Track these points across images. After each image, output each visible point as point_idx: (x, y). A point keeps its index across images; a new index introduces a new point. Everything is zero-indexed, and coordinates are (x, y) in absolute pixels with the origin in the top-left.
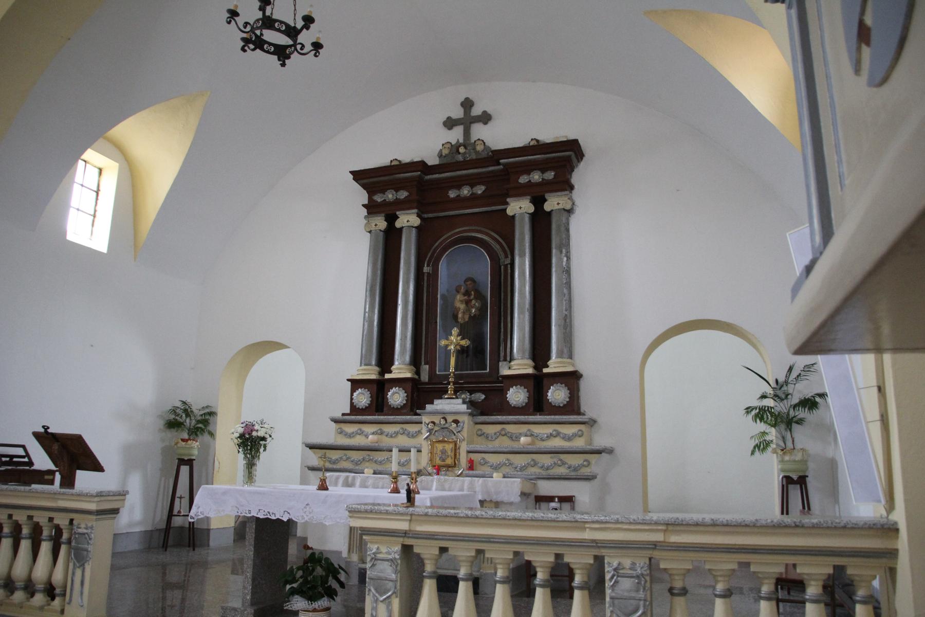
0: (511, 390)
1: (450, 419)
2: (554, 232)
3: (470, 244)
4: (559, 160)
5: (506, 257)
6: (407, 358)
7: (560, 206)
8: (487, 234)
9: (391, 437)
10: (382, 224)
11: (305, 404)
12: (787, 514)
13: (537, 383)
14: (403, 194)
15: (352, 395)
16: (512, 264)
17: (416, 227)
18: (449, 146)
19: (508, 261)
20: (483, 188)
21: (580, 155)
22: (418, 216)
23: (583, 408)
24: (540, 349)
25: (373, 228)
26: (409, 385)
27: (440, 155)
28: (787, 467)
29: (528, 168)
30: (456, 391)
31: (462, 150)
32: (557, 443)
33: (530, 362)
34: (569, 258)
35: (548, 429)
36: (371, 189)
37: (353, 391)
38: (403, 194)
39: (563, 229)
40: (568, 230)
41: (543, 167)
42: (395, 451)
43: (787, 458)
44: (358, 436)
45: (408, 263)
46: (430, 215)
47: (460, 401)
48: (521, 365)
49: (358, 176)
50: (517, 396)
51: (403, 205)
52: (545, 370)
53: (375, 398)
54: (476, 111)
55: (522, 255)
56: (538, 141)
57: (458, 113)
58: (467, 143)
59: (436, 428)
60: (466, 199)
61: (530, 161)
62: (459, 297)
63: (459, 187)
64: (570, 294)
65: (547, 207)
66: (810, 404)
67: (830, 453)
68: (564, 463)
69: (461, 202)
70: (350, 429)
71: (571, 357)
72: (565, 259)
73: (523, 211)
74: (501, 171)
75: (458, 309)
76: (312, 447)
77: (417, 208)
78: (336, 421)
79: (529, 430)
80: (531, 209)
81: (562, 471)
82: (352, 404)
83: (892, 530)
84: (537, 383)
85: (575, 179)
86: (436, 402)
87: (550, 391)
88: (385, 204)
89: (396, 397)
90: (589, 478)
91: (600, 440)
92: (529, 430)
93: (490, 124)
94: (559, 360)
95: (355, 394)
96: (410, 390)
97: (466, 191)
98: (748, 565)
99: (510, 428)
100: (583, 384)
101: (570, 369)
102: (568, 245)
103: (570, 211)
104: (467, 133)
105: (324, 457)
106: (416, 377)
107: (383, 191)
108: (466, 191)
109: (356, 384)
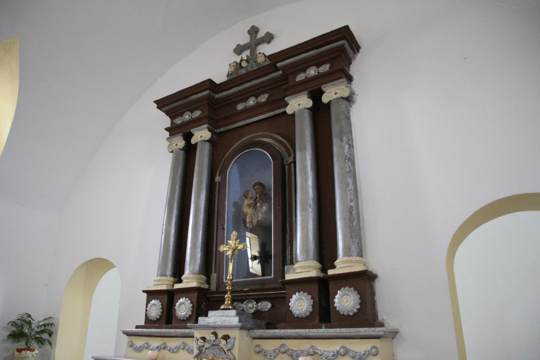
0: (294, 297)
1: (220, 334)
5: (290, 155)
7: (338, 95)
9: (173, 352)
10: (180, 142)
13: (323, 288)
14: (197, 114)
15: (147, 306)
17: (208, 141)
20: (266, 96)
21: (356, 47)
22: (210, 130)
23: (382, 315)
24: (326, 252)
26: (195, 295)
29: (303, 66)
30: (233, 301)
31: (244, 64)
33: (318, 265)
34: (351, 146)
36: (172, 114)
38: (197, 114)
39: (342, 116)
40: (349, 118)
41: (317, 62)
44: (145, 350)
46: (222, 129)
48: (304, 267)
49: (155, 102)
50: (300, 304)
51: (196, 123)
52: (331, 272)
54: (261, 35)
55: (304, 149)
59: (207, 345)
61: (304, 59)
63: (245, 100)
64: (355, 183)
65: (325, 99)
72: (347, 147)
73: (302, 107)
74: (282, 76)
75: (245, 215)
77: (207, 123)
78: (129, 334)
79: (312, 347)
80: (309, 103)
85: (353, 70)
86: (211, 313)
87: (337, 296)
89: (183, 307)
92: (312, 347)
94: (347, 258)
96: (195, 300)
99: (291, 344)
100: (379, 286)
101: (358, 268)
103: (349, 99)
106: (206, 286)
108: (251, 102)
109: (151, 294)
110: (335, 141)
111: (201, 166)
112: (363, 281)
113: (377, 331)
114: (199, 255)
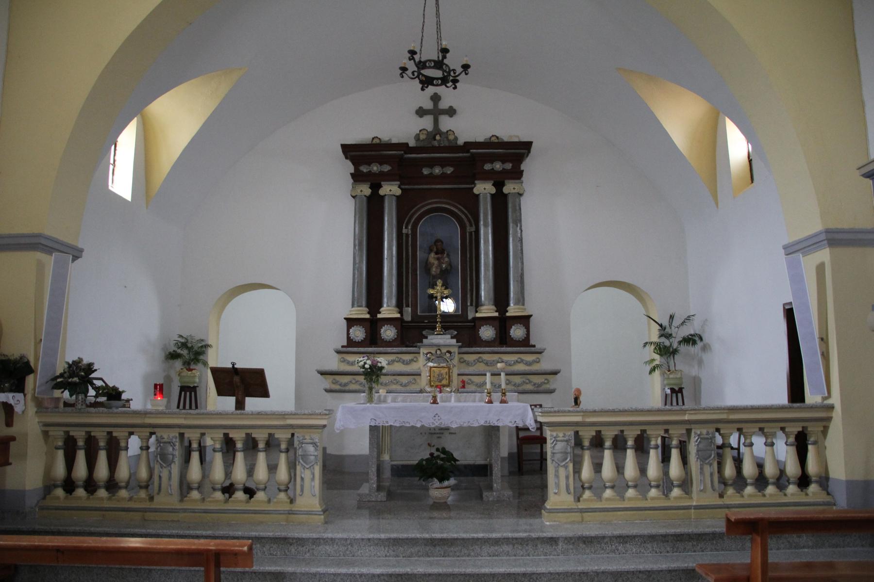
1: (444, 350)
2: (510, 210)
3: (437, 216)
4: (515, 153)
6: (394, 301)
7: (516, 191)
8: (457, 208)
10: (366, 190)
11: (297, 340)
12: (197, 407)
13: (503, 323)
14: (386, 168)
16: (477, 232)
18: (425, 132)
19: (473, 229)
22: (399, 187)
23: (532, 342)
24: (501, 298)
25: (358, 192)
27: (417, 138)
28: (672, 382)
29: (492, 159)
32: (521, 367)
33: (494, 308)
35: (514, 358)
36: (356, 161)
37: (349, 327)
38: (386, 168)
41: (503, 159)
42: (488, 374)
43: (671, 376)
45: (390, 224)
47: (449, 336)
48: (488, 310)
49: (348, 150)
50: (487, 333)
51: (388, 177)
52: (379, 316)
53: (368, 332)
56: (497, 138)
57: (428, 105)
58: (437, 130)
60: (437, 177)
61: (494, 153)
62: (433, 255)
63: (431, 166)
66: (690, 340)
67: (694, 371)
68: (530, 382)
69: (432, 178)
70: (351, 358)
71: (523, 305)
73: (486, 191)
76: (323, 373)
80: (493, 190)
81: (529, 387)
82: (348, 338)
83: (831, 408)
84: (503, 323)
88: (370, 174)
89: (388, 333)
90: (551, 392)
91: (545, 365)
93: (455, 117)
95: (351, 331)
97: (437, 171)
98: (111, 432)
99: (486, 357)
102: (520, 221)
103: (521, 195)
104: (436, 122)
105: (335, 382)
107: (369, 164)
108: (437, 171)
109: (351, 322)
110: (511, 225)
111: (390, 214)
112: (525, 320)
113: (533, 349)
114: (394, 272)
